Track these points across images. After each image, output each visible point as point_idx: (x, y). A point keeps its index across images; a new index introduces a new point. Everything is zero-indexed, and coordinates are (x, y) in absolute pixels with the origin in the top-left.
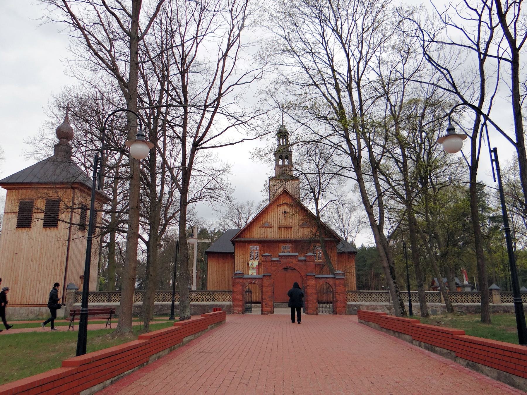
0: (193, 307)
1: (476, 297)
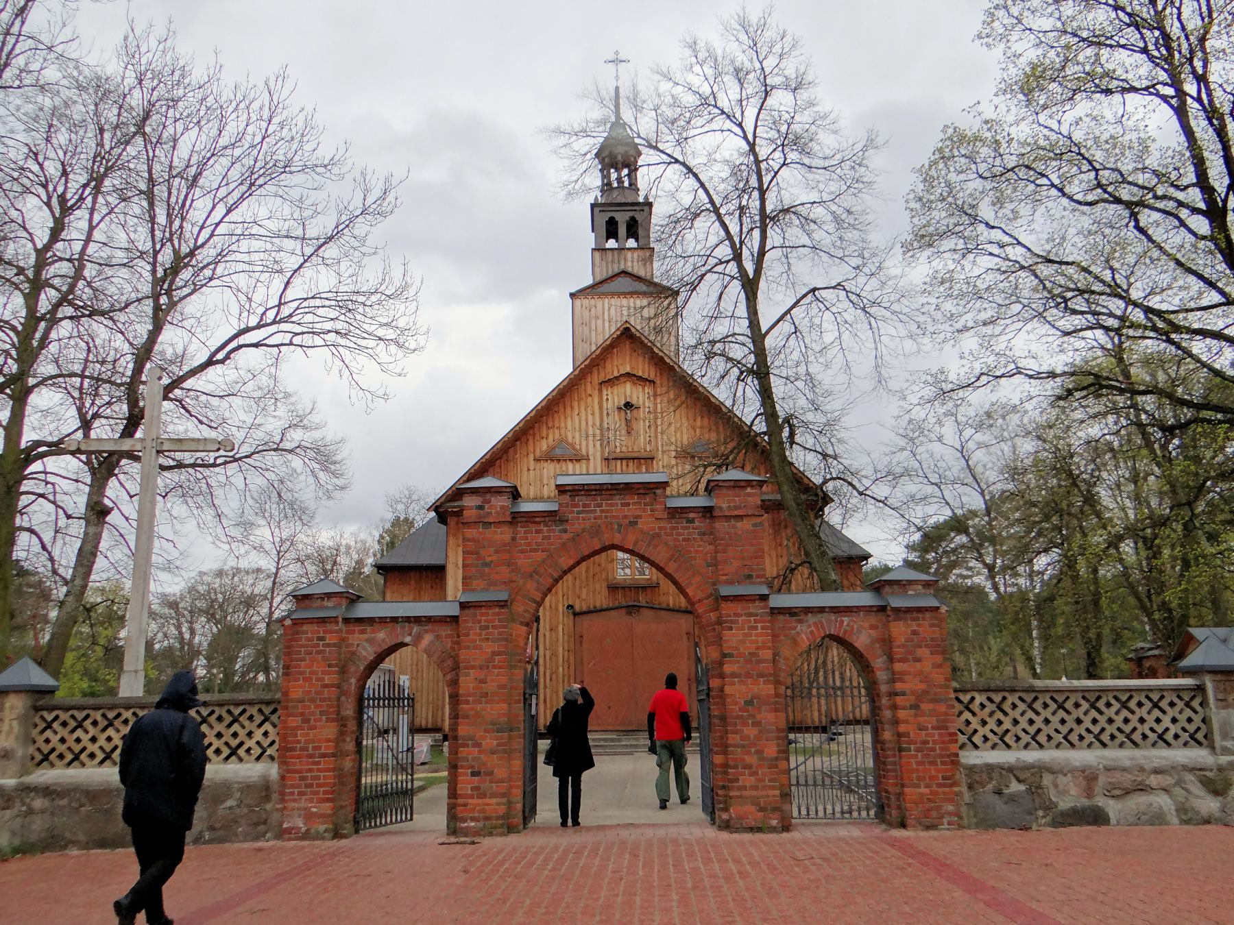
0: (38, 803)
1: (1046, 713)
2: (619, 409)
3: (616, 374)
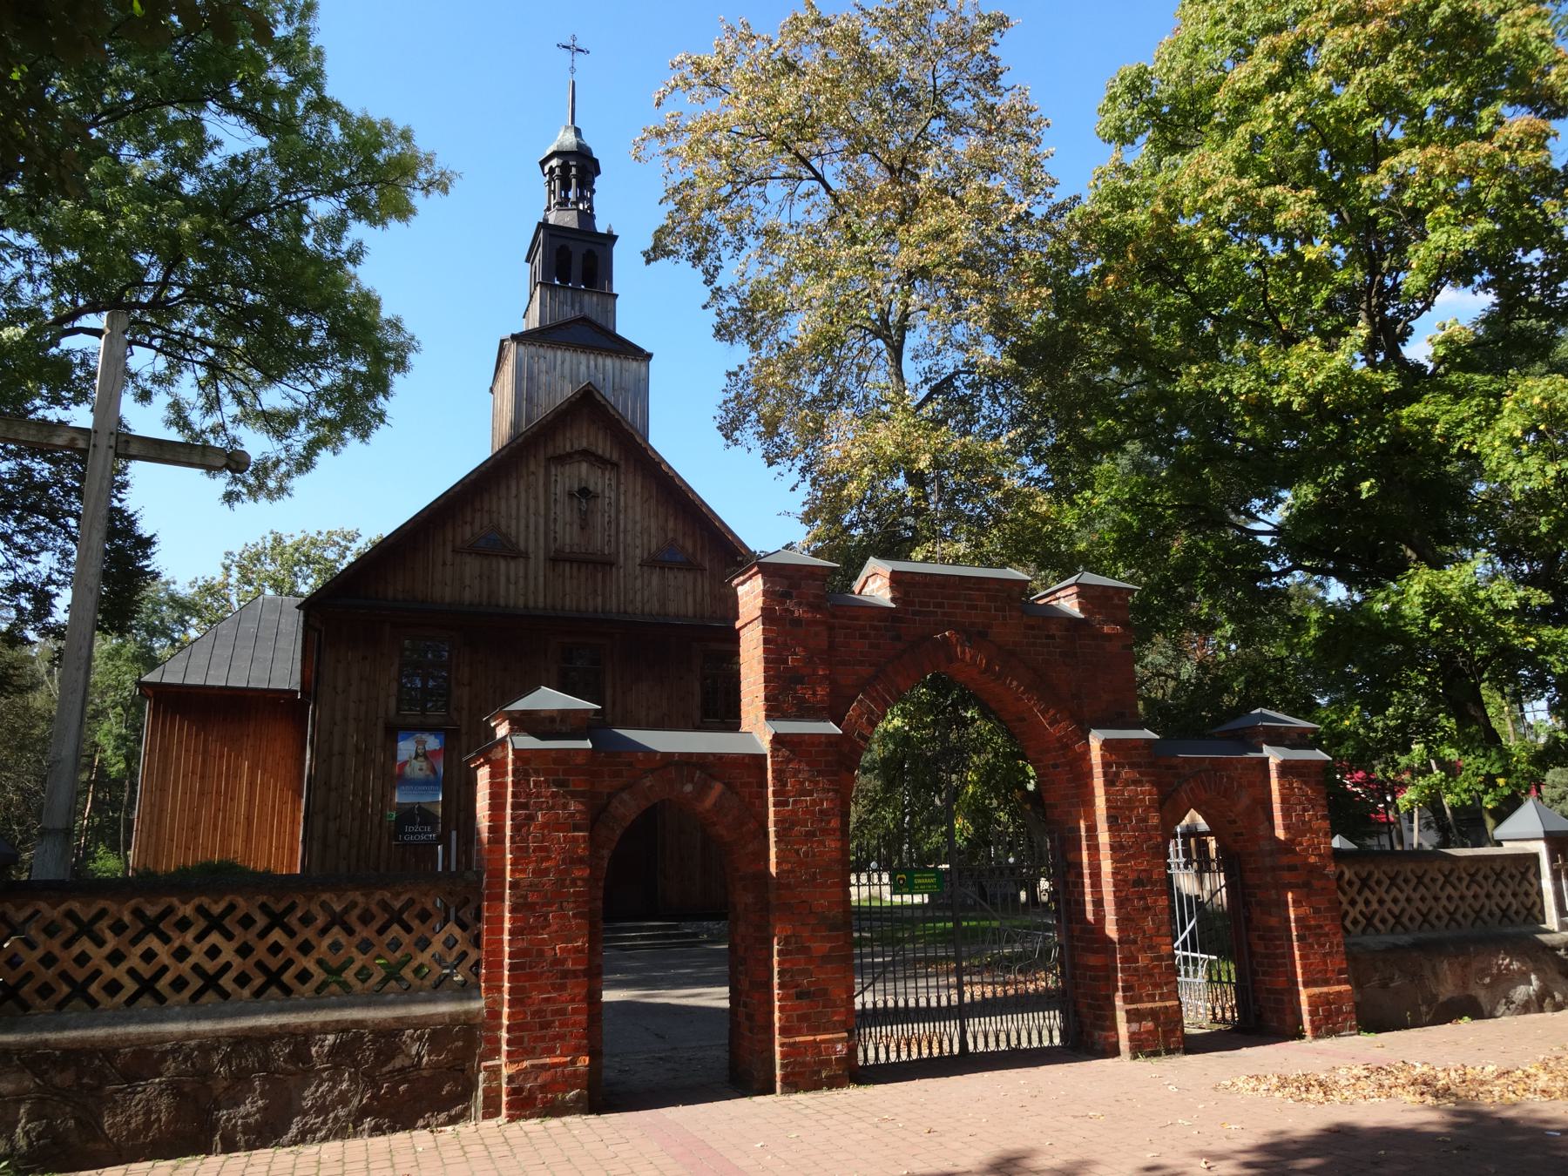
2: (571, 495)
3: (568, 449)
